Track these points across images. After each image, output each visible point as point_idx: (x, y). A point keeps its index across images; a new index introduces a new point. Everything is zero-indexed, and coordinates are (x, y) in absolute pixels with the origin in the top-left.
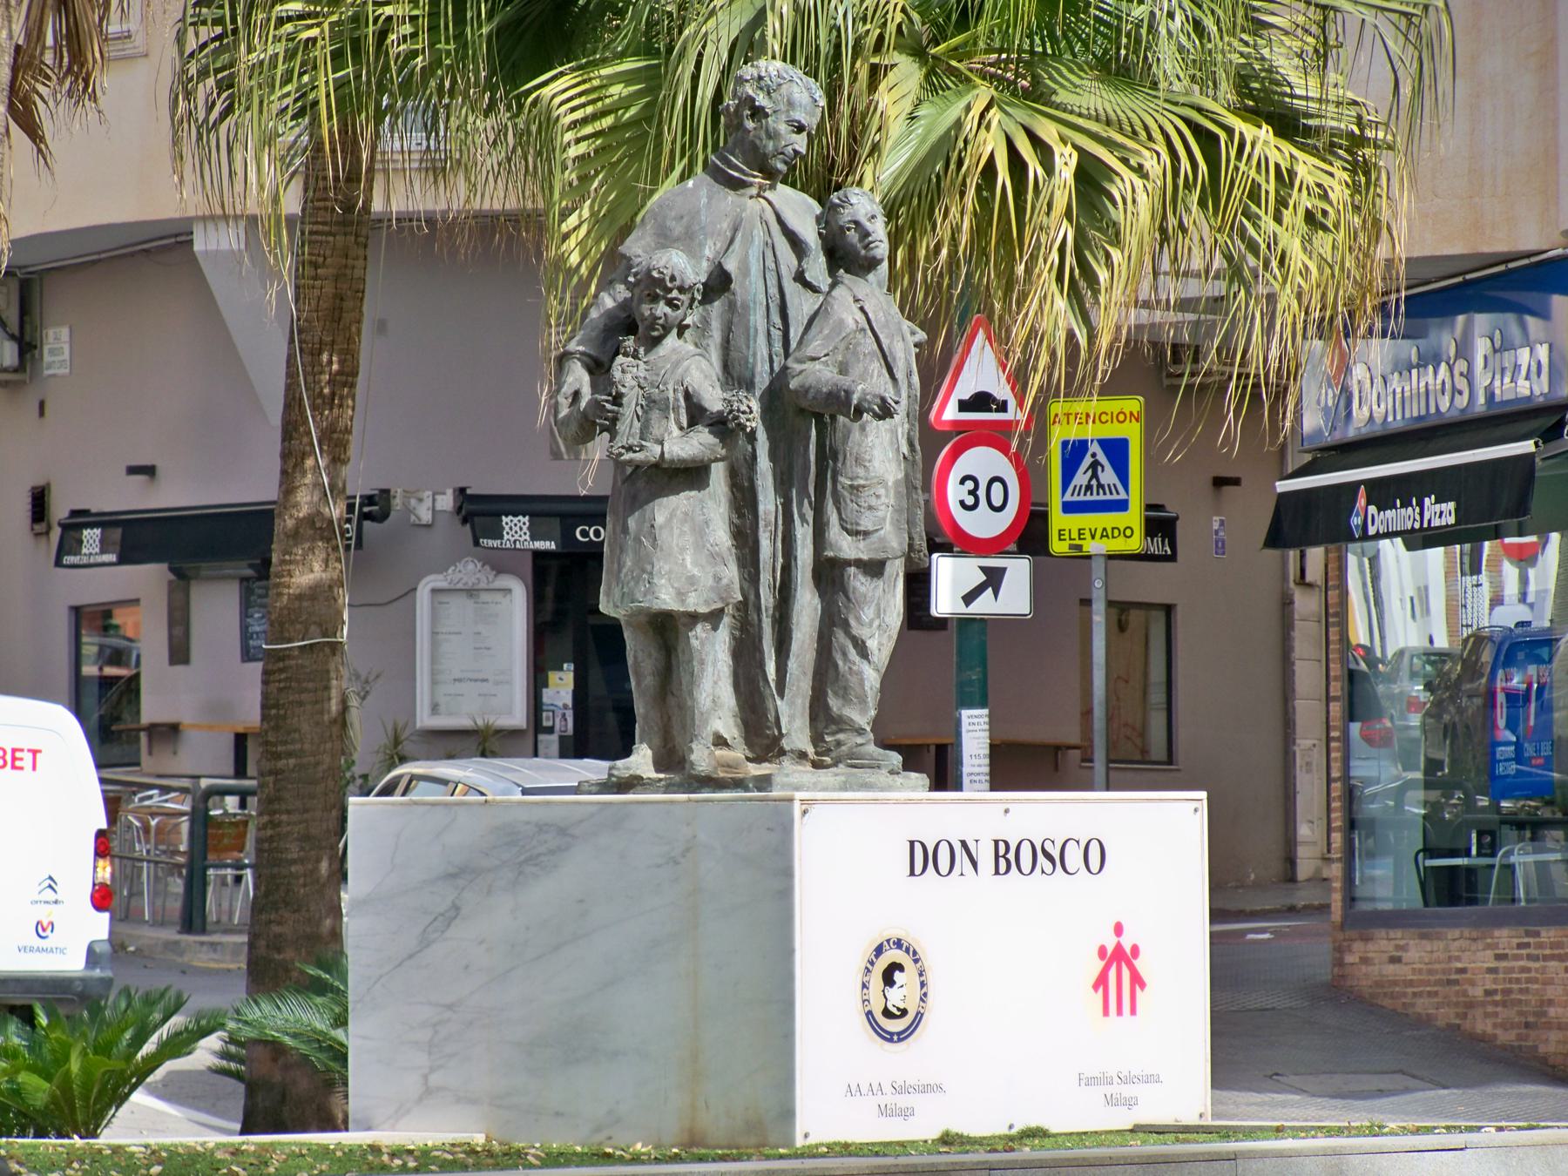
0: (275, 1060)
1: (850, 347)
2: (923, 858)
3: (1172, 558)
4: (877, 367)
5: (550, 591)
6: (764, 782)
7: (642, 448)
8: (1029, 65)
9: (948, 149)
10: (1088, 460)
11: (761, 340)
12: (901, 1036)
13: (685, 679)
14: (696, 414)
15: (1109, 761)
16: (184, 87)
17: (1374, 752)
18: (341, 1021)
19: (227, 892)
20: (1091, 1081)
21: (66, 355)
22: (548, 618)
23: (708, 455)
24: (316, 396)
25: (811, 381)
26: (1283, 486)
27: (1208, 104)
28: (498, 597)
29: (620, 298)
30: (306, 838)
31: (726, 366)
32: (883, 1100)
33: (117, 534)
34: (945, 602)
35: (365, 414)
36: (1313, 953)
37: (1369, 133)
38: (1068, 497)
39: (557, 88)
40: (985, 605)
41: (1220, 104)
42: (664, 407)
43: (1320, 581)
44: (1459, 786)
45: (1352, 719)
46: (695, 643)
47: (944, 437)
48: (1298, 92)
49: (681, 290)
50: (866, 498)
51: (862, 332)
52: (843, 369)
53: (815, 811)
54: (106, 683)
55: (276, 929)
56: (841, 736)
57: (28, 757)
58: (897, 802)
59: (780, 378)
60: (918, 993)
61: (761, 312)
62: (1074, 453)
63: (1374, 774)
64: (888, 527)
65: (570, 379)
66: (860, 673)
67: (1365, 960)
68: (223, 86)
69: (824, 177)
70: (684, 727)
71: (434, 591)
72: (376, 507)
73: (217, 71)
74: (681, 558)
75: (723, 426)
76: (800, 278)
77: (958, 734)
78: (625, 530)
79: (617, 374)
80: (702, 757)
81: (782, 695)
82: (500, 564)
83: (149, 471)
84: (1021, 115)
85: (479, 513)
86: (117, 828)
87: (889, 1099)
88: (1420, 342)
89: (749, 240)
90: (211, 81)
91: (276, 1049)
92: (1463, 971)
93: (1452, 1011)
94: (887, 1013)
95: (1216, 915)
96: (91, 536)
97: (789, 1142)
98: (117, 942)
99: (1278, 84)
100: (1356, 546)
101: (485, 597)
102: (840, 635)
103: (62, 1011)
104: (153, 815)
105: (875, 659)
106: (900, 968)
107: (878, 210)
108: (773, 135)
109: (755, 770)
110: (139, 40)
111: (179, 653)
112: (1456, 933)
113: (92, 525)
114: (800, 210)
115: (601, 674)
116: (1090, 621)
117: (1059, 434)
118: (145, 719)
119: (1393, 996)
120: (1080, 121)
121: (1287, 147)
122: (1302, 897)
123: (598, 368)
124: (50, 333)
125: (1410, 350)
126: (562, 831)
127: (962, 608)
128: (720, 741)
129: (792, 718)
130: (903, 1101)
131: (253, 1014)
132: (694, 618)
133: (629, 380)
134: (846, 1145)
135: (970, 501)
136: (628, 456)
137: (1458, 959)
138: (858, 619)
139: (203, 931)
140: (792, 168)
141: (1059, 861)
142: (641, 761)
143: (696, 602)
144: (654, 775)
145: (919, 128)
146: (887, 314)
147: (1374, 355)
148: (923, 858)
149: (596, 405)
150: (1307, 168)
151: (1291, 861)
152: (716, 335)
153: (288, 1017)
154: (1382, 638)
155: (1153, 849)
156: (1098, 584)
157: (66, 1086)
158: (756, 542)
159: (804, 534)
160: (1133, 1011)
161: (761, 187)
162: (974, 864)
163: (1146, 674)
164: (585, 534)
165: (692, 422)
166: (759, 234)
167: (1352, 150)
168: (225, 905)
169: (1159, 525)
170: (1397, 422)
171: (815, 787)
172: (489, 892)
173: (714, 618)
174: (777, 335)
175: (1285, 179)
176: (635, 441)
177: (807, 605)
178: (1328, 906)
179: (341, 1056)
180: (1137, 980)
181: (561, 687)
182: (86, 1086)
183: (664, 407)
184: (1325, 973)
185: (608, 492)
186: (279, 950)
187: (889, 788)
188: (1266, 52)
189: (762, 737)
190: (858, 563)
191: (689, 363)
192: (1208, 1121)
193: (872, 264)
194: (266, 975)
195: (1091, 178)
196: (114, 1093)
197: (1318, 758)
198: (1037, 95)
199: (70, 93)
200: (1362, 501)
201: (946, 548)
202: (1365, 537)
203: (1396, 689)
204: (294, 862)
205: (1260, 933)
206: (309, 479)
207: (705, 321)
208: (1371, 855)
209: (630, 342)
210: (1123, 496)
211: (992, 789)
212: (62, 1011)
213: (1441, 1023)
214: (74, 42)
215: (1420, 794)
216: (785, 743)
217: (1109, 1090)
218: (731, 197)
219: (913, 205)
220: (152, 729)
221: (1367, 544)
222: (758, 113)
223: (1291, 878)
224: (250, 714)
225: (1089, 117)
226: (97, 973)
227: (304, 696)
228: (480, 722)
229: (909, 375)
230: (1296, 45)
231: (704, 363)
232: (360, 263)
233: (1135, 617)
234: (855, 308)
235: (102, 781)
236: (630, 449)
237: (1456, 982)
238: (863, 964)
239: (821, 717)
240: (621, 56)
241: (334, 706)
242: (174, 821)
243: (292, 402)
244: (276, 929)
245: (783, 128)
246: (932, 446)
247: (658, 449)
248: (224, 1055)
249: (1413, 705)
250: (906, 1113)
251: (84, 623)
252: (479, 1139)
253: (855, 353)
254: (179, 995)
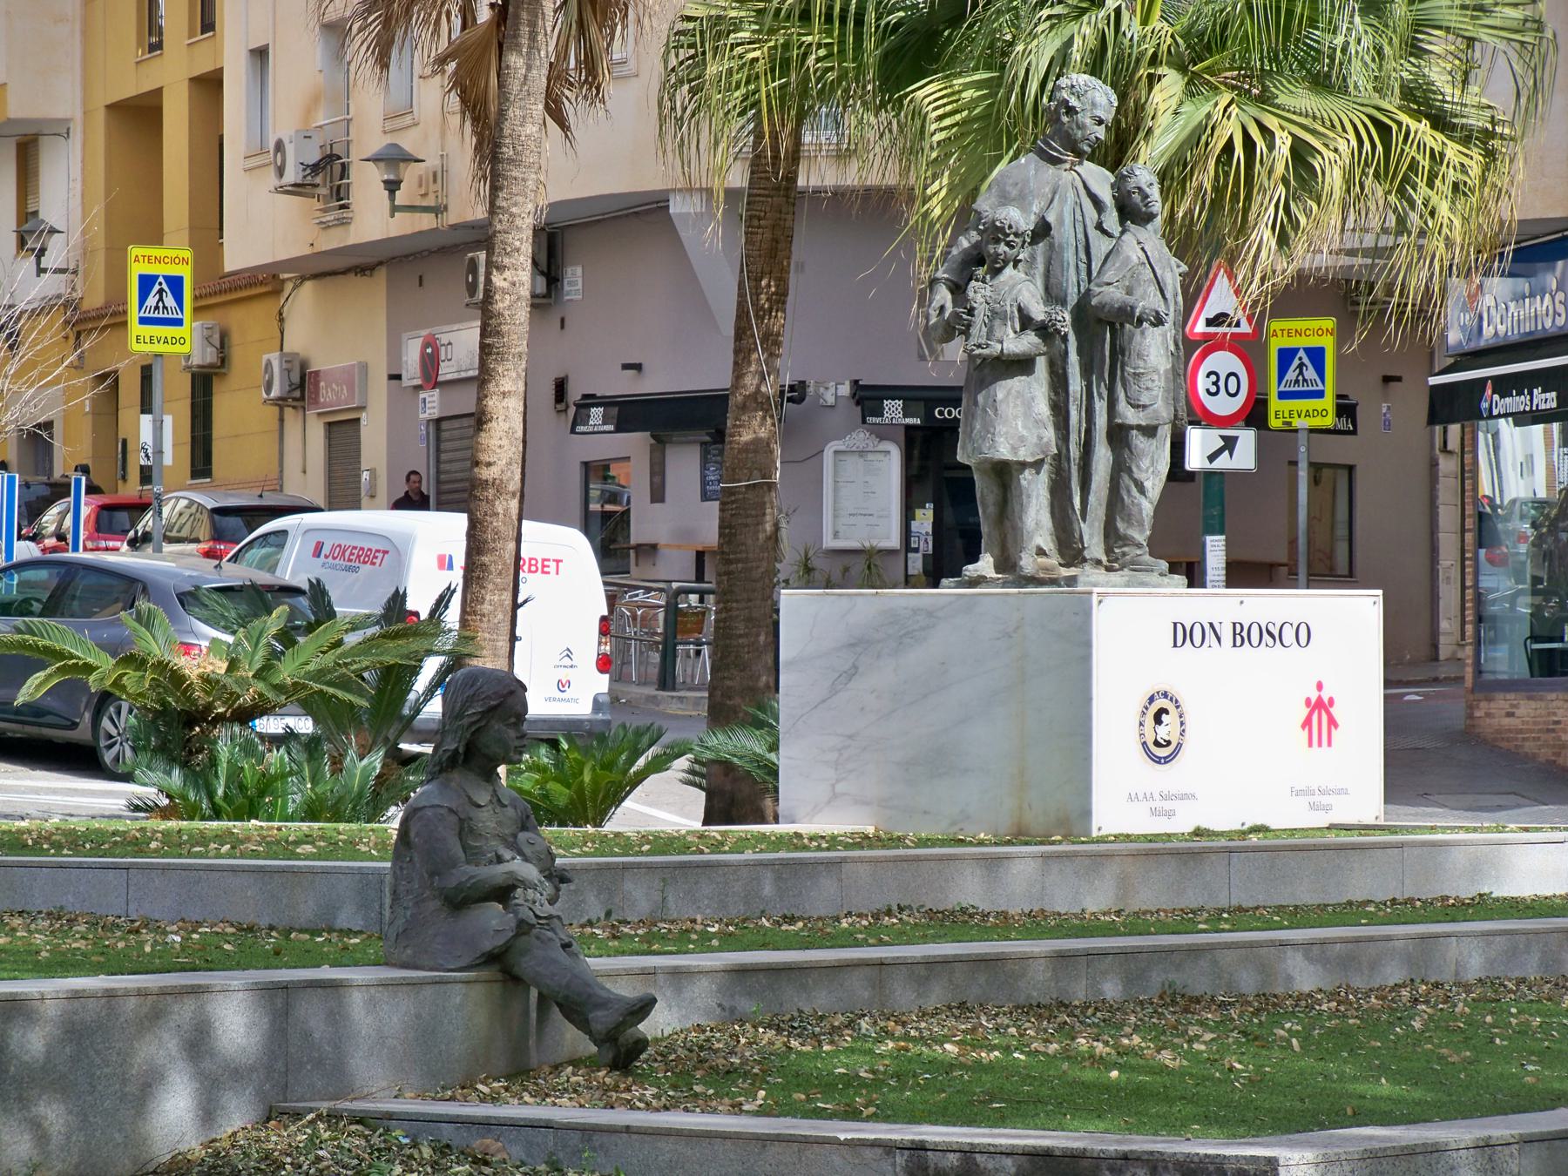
0: (726, 775)
1: (1134, 276)
2: (1183, 635)
3: (1354, 432)
4: (1153, 290)
5: (916, 453)
6: (1071, 581)
7: (988, 346)
8: (1261, 79)
9: (1198, 137)
10: (1296, 362)
11: (1072, 270)
12: (1167, 760)
13: (1017, 508)
14: (1026, 322)
15: (1310, 575)
16: (668, 89)
17: (1496, 569)
18: (774, 747)
19: (690, 662)
21: (580, 286)
22: (914, 472)
23: (1034, 351)
24: (758, 309)
25: (1107, 299)
26: (1434, 381)
27: (1385, 105)
28: (880, 457)
29: (973, 241)
30: (749, 619)
31: (1047, 289)
32: (1153, 805)
33: (615, 411)
34: (1195, 460)
35: (787, 323)
36: (1452, 710)
37: (1499, 130)
38: (1282, 388)
39: (927, 92)
40: (1223, 462)
41: (1391, 103)
42: (1004, 317)
43: (1458, 450)
44: (1556, 594)
45: (1480, 546)
46: (1024, 483)
47: (1196, 344)
48: (1448, 99)
49: (1016, 235)
50: (1145, 382)
51: (1142, 264)
52: (1129, 292)
53: (1107, 600)
54: (606, 516)
55: (729, 683)
56: (1126, 549)
57: (553, 565)
58: (1165, 595)
59: (1085, 297)
61: (1072, 250)
62: (1286, 356)
63: (1494, 585)
64: (1160, 402)
65: (938, 297)
66: (1139, 505)
67: (1488, 715)
68: (693, 92)
69: (1116, 149)
70: (1015, 541)
71: (836, 452)
72: (797, 393)
73: (690, 81)
74: (1016, 423)
75: (1045, 331)
76: (1099, 227)
77: (1204, 554)
78: (976, 403)
79: (971, 294)
80: (1028, 563)
81: (1084, 520)
82: (882, 434)
83: (637, 367)
84: (1253, 110)
85: (868, 399)
86: (614, 617)
87: (1158, 804)
88: (1533, 280)
89: (1063, 200)
90: (686, 87)
91: (726, 766)
92: (1558, 722)
93: (1550, 752)
94: (1157, 744)
95: (1388, 683)
96: (596, 413)
97: (1088, 832)
98: (614, 697)
99: (1434, 93)
100: (1482, 423)
101: (870, 457)
102: (1125, 478)
103: (579, 742)
104: (639, 607)
105: (1150, 495)
106: (1166, 711)
107: (1155, 179)
108: (1081, 127)
109: (1065, 572)
110: (632, 64)
111: (658, 495)
112: (1553, 696)
113: (597, 405)
114: (1100, 179)
115: (956, 512)
116: (1296, 476)
117: (1276, 344)
118: (633, 541)
119: (1508, 740)
120: (1294, 117)
121: (1440, 136)
122: (1443, 672)
123: (958, 290)
124: (569, 270)
125: (1523, 285)
126: (930, 614)
127: (1207, 465)
128: (1041, 552)
129: (1091, 536)
130: (1168, 805)
131: (712, 741)
132: (1023, 465)
133: (979, 299)
134: (1128, 836)
135: (1213, 389)
136: (978, 351)
137: (1555, 714)
138: (1138, 467)
139: (674, 689)
140: (1093, 151)
141: (1278, 638)
142: (985, 565)
143: (1024, 455)
144: (995, 576)
145: (1181, 120)
146: (1160, 252)
147: (1498, 287)
148: (1183, 635)
149: (956, 315)
150: (1452, 151)
151: (1435, 646)
152: (1040, 267)
153: (740, 744)
154: (1501, 491)
155: (1346, 629)
156: (1303, 449)
157: (581, 790)
158: (1068, 412)
159: (1101, 407)
160: (1330, 744)
161: (1073, 163)
162: (1219, 639)
163: (1333, 514)
164: (941, 413)
165: (1023, 328)
166: (1071, 195)
167: (1483, 139)
168: (689, 671)
169: (1345, 409)
170: (1514, 336)
171: (1107, 585)
172: (878, 657)
173: (1037, 465)
174: (1083, 266)
175: (1437, 158)
176: (983, 341)
177: (1103, 456)
178: (1463, 678)
179: (773, 772)
180: (1333, 723)
181: (924, 521)
182: (595, 792)
183: (1004, 317)
184: (1460, 723)
185: (962, 384)
186: (730, 698)
187: (1159, 586)
188: (1426, 71)
189: (1071, 551)
190: (1139, 428)
191: (1021, 287)
192: (1381, 822)
193: (1150, 217)
194: (721, 714)
195: (1301, 153)
196: (615, 795)
197: (1455, 574)
198: (1265, 99)
199: (585, 97)
200: (1489, 391)
201: (1195, 423)
202: (1491, 416)
203: (1510, 526)
204: (741, 636)
205: (1412, 696)
206: (753, 368)
207: (1033, 257)
208: (1493, 642)
209: (980, 272)
210: (1320, 387)
212: (579, 742)
213: (1542, 759)
214: (590, 65)
215: (1529, 599)
216: (1087, 554)
217: (1312, 799)
218: (1051, 170)
219: (1173, 175)
220: (638, 547)
221: (1491, 422)
222: (1071, 111)
223: (1436, 659)
224: (710, 536)
225: (1300, 114)
226: (600, 716)
227: (749, 521)
228: (867, 545)
229: (1176, 295)
230: (1449, 67)
231: (1032, 287)
232: (789, 217)
233: (1326, 473)
234: (1138, 248)
235: (605, 584)
236: (979, 346)
237: (1553, 731)
238: (1141, 709)
239: (1112, 536)
240: (976, 69)
241: (768, 527)
242: (653, 612)
243: (742, 314)
244: (729, 683)
245: (1088, 121)
246: (1190, 349)
247: (999, 347)
248: (691, 772)
249: (1522, 538)
250: (1170, 814)
251: (591, 475)
252: (870, 830)
253: (1138, 280)
254: (660, 729)
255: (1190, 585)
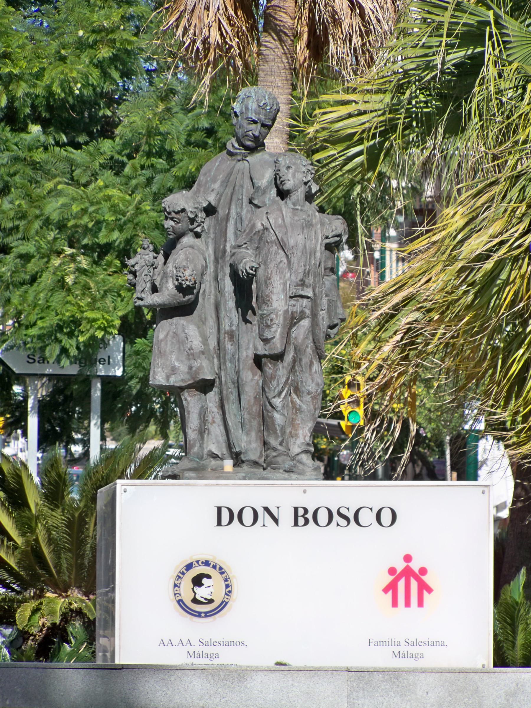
20: (382, 643)
60: (223, 590)
94: (195, 601)
160: (421, 604)
180: (424, 587)
211: (324, 480)
217: (396, 649)
245: (245, 123)
255: (459, 478)
